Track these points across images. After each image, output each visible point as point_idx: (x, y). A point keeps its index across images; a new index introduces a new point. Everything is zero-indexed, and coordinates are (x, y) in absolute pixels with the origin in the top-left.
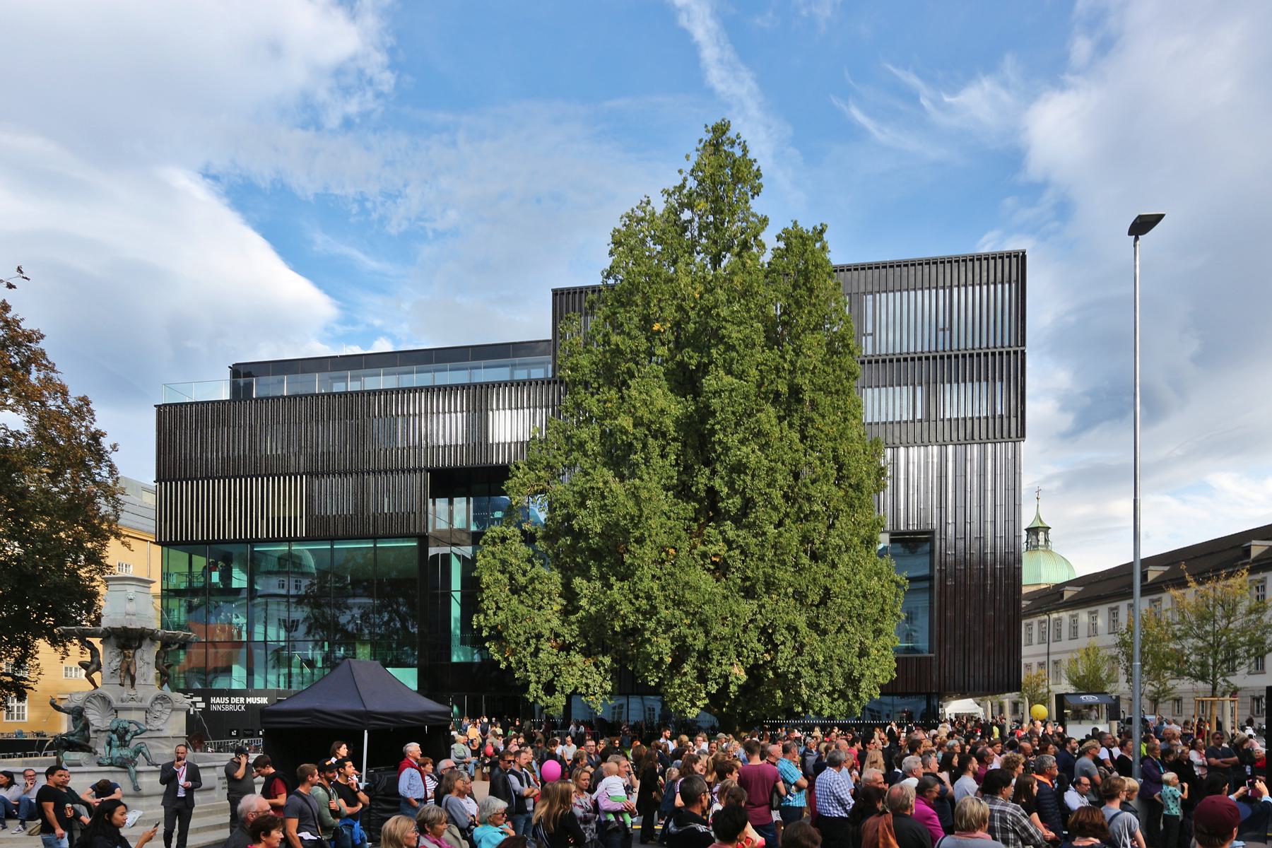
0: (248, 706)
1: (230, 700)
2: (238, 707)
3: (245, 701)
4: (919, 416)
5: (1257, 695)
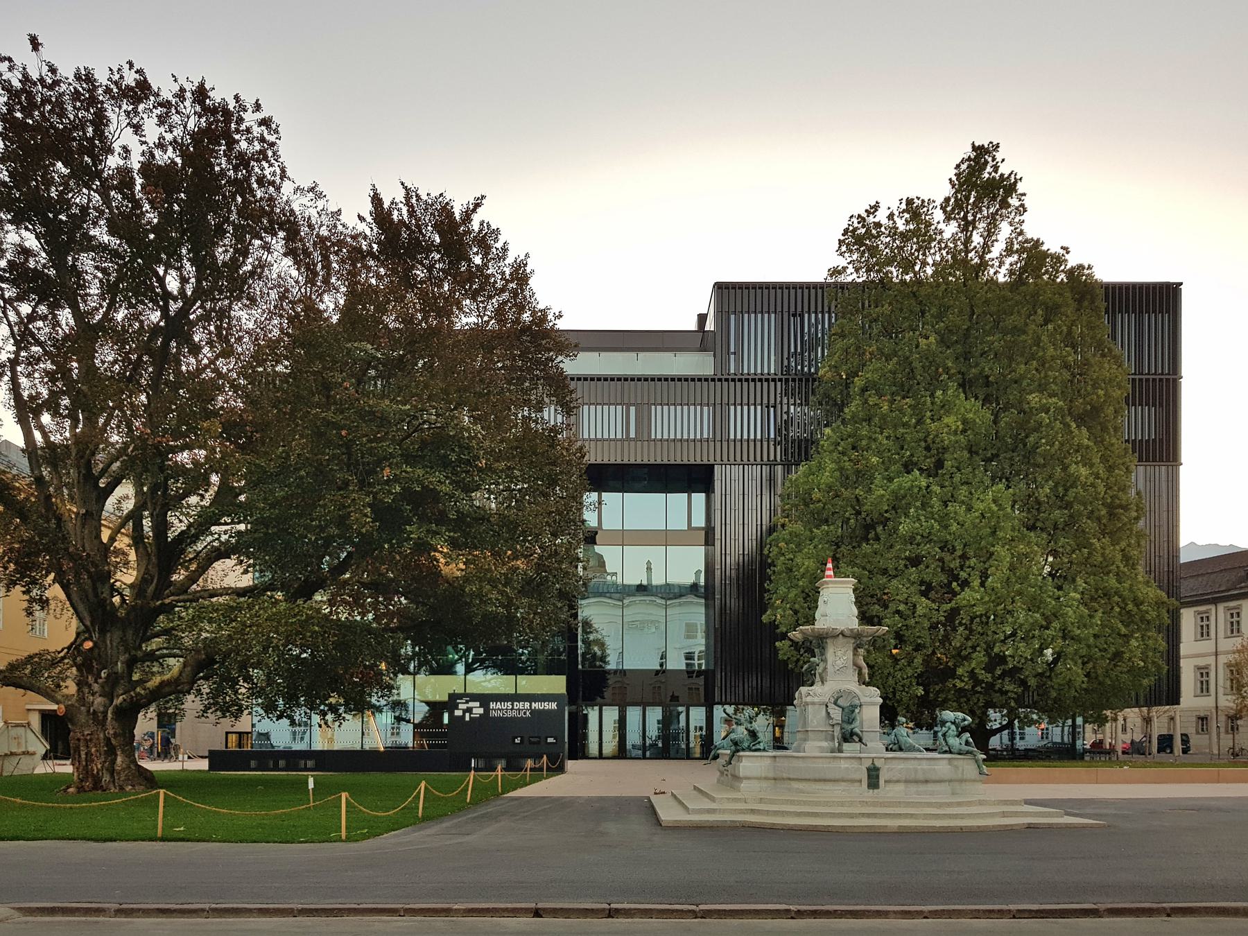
0: (533, 712)
1: (513, 705)
2: (522, 713)
3: (530, 706)
4: (632, 435)
5: (1202, 715)
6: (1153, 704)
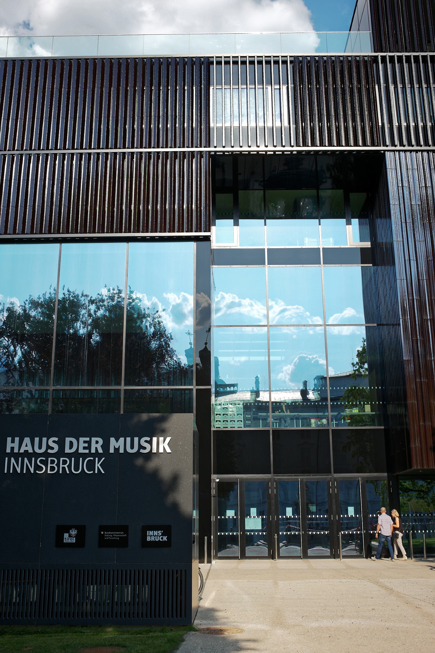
1: (61, 444)
3: (106, 446)
6: (42, 65)
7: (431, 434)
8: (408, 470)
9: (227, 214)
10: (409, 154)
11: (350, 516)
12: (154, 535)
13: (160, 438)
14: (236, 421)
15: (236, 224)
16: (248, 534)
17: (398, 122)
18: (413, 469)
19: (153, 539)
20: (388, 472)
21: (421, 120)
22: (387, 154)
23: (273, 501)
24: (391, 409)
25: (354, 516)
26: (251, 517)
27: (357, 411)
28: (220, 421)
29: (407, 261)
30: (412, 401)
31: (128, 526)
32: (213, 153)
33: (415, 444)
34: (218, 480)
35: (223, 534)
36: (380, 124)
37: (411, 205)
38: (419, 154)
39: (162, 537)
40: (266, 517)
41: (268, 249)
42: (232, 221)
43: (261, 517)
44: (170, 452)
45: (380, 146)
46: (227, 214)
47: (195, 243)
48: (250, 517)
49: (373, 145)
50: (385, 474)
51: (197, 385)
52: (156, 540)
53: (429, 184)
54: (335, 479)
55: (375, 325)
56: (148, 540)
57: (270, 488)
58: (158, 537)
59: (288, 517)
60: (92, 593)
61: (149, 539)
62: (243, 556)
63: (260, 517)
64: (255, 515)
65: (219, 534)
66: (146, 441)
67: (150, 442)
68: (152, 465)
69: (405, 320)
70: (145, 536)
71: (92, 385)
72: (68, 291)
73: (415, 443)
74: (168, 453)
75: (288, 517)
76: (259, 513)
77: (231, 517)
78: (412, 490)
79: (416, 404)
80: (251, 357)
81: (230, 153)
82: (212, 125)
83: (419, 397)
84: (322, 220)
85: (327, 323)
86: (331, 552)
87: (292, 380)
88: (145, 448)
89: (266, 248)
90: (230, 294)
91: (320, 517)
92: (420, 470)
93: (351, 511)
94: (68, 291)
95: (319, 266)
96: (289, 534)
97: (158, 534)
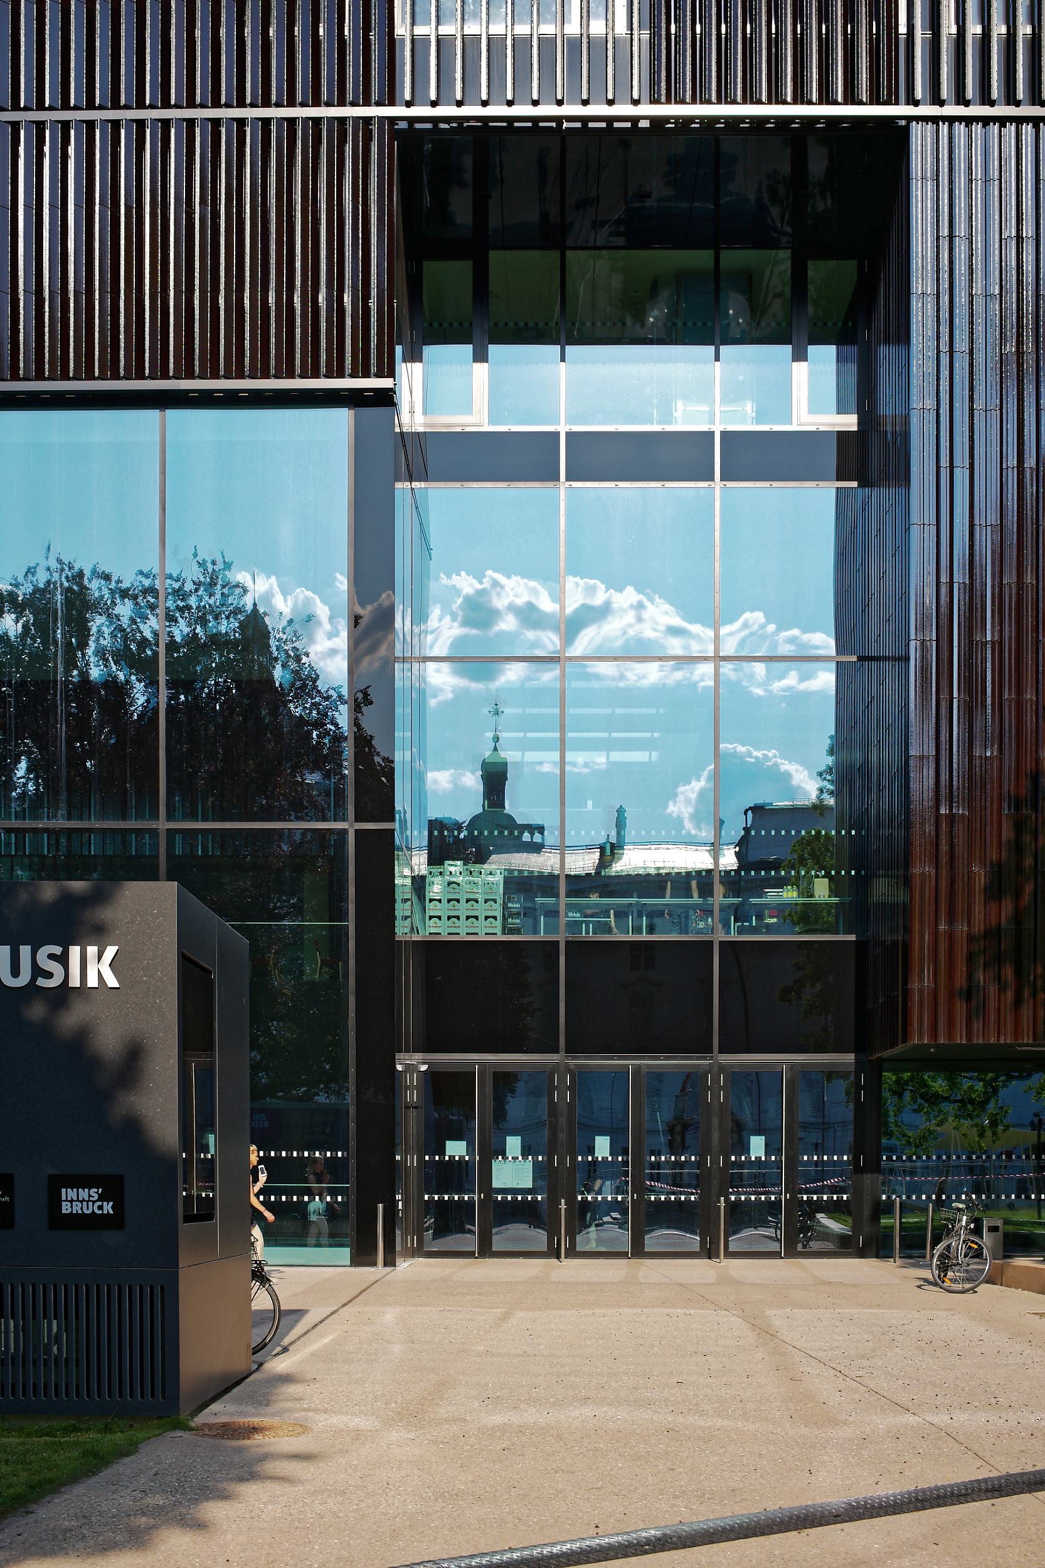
7: (965, 955)
8: (899, 1049)
9: (456, 325)
10: (979, 131)
11: (753, 1159)
12: (80, 1199)
13: (88, 947)
14: (463, 918)
15: (480, 356)
16: (499, 1198)
17: (957, 23)
18: (910, 1043)
19: (77, 1208)
20: (856, 1052)
21: (1025, 14)
22: (916, 129)
23: (563, 1121)
24: (881, 889)
25: (763, 1159)
26: (508, 1158)
27: (795, 894)
28: (439, 918)
29: (943, 471)
30: (922, 868)
31: (12, 1175)
32: (403, 125)
33: (922, 982)
34: (424, 1068)
35: (456, 1198)
36: (903, 29)
37: (971, 295)
38: (1010, 129)
39: (100, 1203)
40: (545, 1157)
41: (569, 435)
42: (469, 348)
43: (532, 1159)
44: (118, 986)
45: (897, 103)
46: (456, 325)
47: (352, 412)
48: (505, 1158)
49: (875, 100)
50: (850, 1057)
51: (358, 819)
52: (86, 1211)
53: (1028, 231)
54: (722, 1068)
55: (854, 659)
56: (64, 1211)
57: (569, 1088)
58: (90, 1204)
59: (600, 1159)
60: (12, 1335)
61: (66, 1208)
62: (486, 1250)
63: (530, 1158)
64: (518, 1153)
65: (426, 1197)
66: (52, 957)
67: (63, 960)
68: (71, 1019)
69: (923, 642)
70: (55, 1202)
71: (124, 818)
72: (59, 561)
73: (921, 979)
74: (110, 988)
75: (600, 1159)
76: (527, 1150)
77: (457, 1158)
78: (947, 1099)
79: (934, 876)
80: (647, 759)
81: (454, 125)
82: (401, 29)
83: (944, 859)
84: (723, 349)
85: (723, 651)
86: (703, 1242)
87: (696, 818)
88: (49, 975)
89: (563, 429)
90: (518, 578)
91: (748, 1159)
92: (928, 1046)
93: (757, 1146)
94: (59, 561)
95: (710, 487)
96: (204, 1195)
97: (90, 1196)
